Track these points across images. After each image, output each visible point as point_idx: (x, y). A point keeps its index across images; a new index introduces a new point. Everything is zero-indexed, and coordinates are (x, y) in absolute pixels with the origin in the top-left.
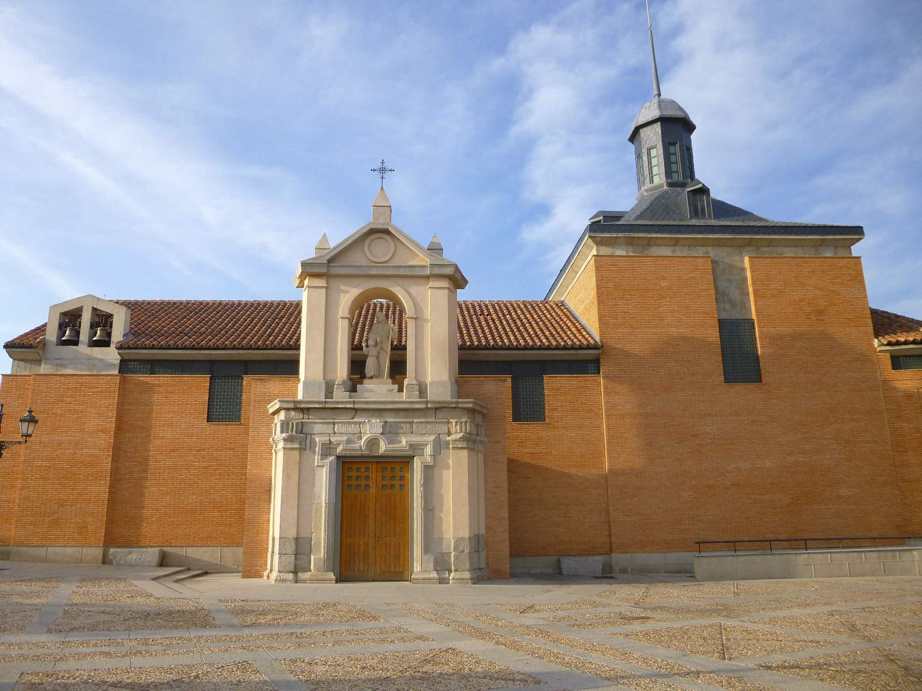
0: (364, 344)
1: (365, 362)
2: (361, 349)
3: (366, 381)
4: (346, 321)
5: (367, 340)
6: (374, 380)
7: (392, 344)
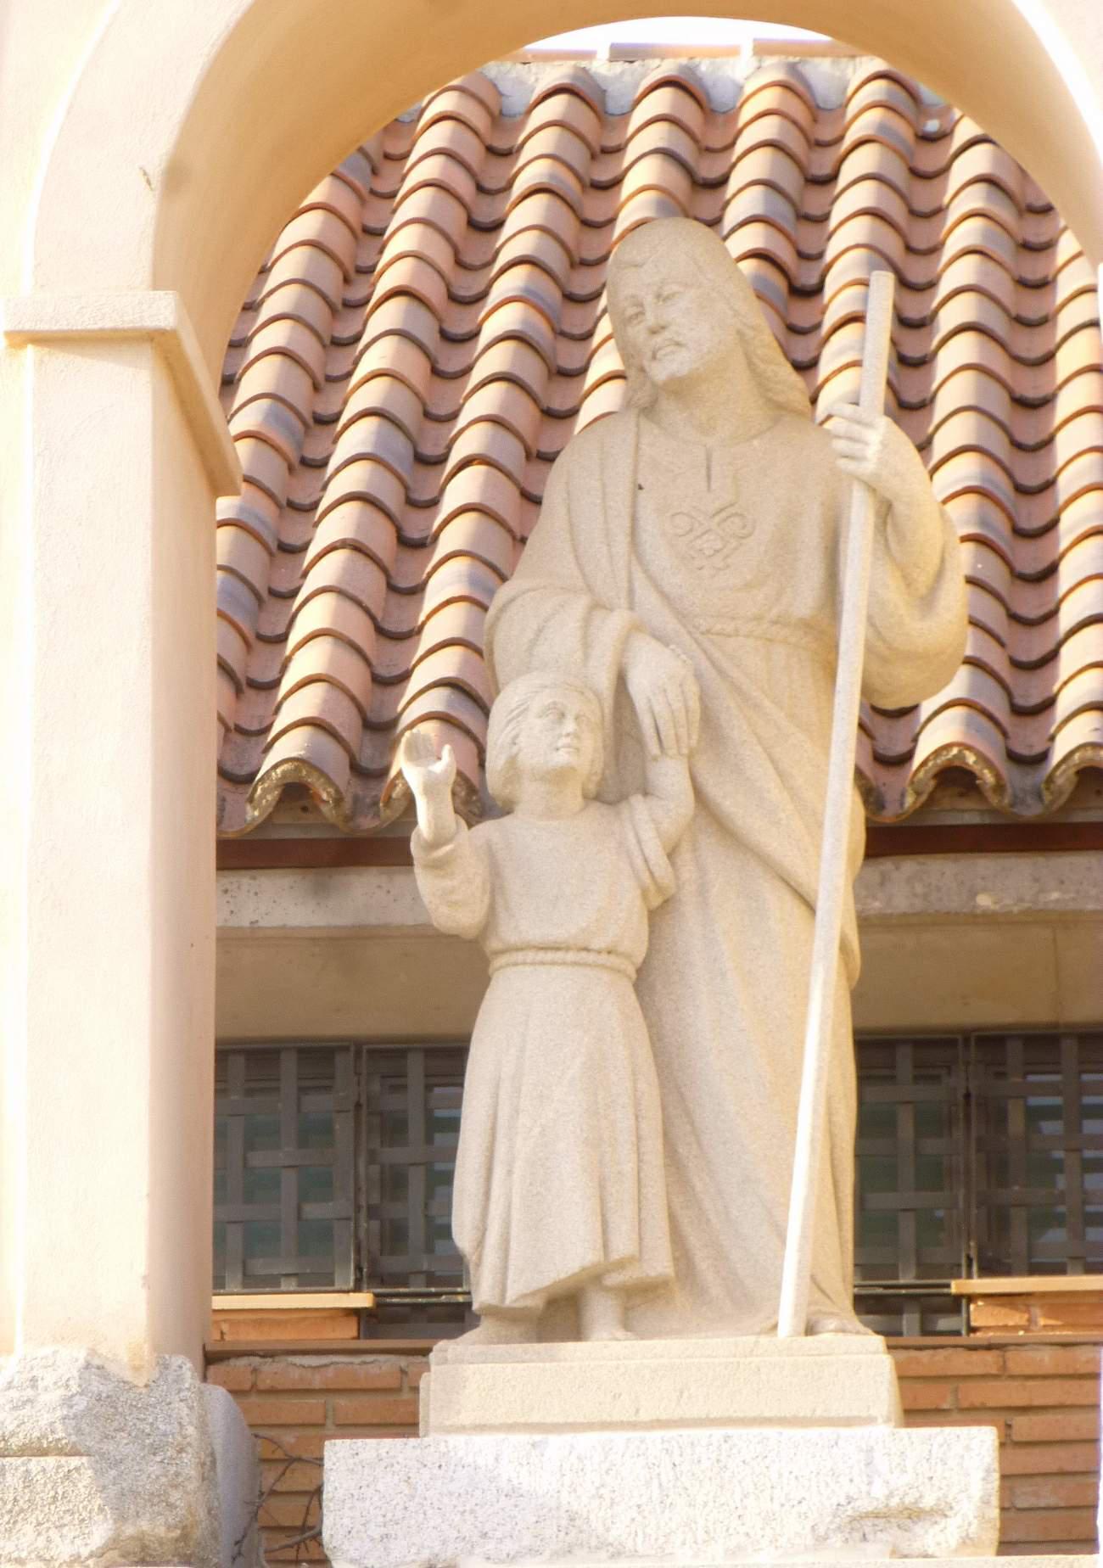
0: (422, 770)
1: (447, 1058)
2: (385, 847)
3: (465, 1376)
4: (129, 398)
5: (471, 701)
6: (603, 1356)
7: (883, 759)
